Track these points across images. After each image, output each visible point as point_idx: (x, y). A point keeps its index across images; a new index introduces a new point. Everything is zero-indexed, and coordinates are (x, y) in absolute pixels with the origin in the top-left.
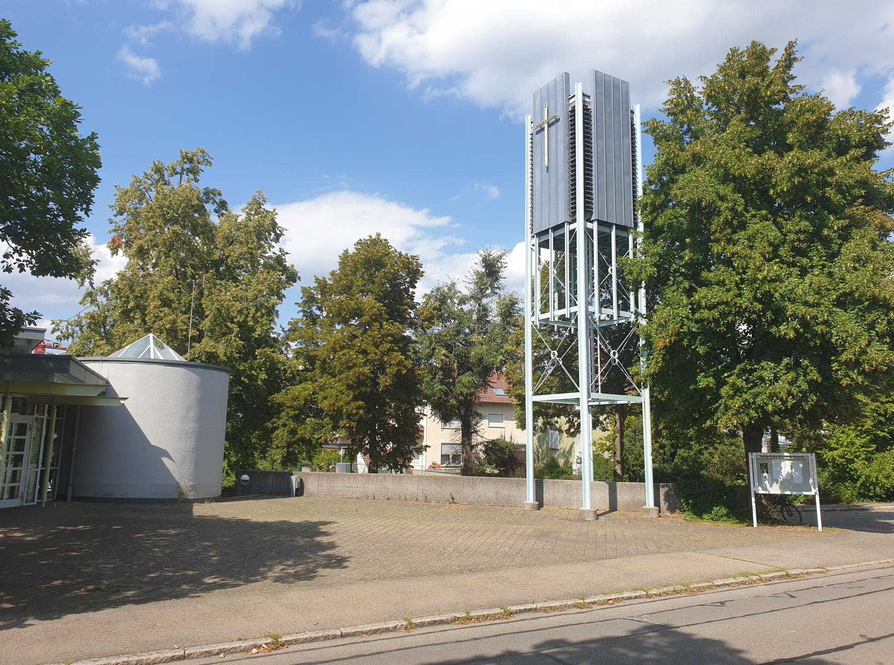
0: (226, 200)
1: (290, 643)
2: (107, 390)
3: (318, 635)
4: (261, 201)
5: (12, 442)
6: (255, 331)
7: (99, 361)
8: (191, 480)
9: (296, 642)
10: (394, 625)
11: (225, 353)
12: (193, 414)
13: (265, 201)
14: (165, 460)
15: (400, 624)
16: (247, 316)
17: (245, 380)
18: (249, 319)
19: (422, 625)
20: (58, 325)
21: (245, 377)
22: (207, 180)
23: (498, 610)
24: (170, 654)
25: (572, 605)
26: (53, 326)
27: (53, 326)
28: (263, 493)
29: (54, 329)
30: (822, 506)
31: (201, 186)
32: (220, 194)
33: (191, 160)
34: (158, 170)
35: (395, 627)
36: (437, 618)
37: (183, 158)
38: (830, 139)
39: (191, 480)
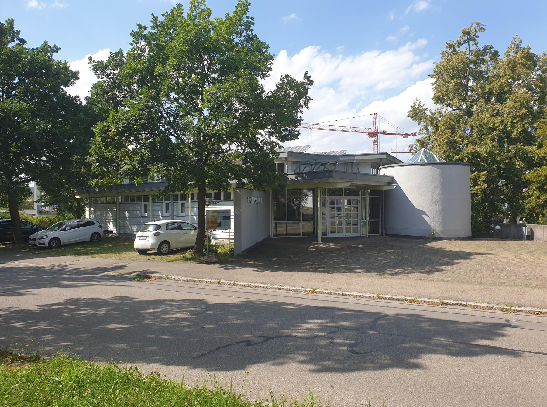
0: (497, 50)
1: (319, 292)
2: (392, 181)
3: (331, 292)
4: (517, 43)
5: (187, 200)
6: (512, 133)
7: (388, 167)
8: (441, 227)
9: (322, 293)
10: (369, 295)
11: (486, 151)
12: (438, 191)
13: (522, 42)
14: (424, 216)
15: (372, 296)
16: (507, 124)
17: (503, 166)
18: (508, 126)
19: (385, 298)
20: (412, 147)
21: (503, 165)
22: (483, 41)
23: (438, 301)
24: (276, 287)
25: (498, 308)
26: (410, 148)
27: (410, 148)
28: (509, 237)
29: (411, 149)
30: (228, 215)
31: (481, 46)
32: (492, 48)
33: (469, 33)
34: (450, 46)
35: (370, 297)
36: (395, 297)
37: (464, 34)
38: (139, 30)
39: (441, 227)
